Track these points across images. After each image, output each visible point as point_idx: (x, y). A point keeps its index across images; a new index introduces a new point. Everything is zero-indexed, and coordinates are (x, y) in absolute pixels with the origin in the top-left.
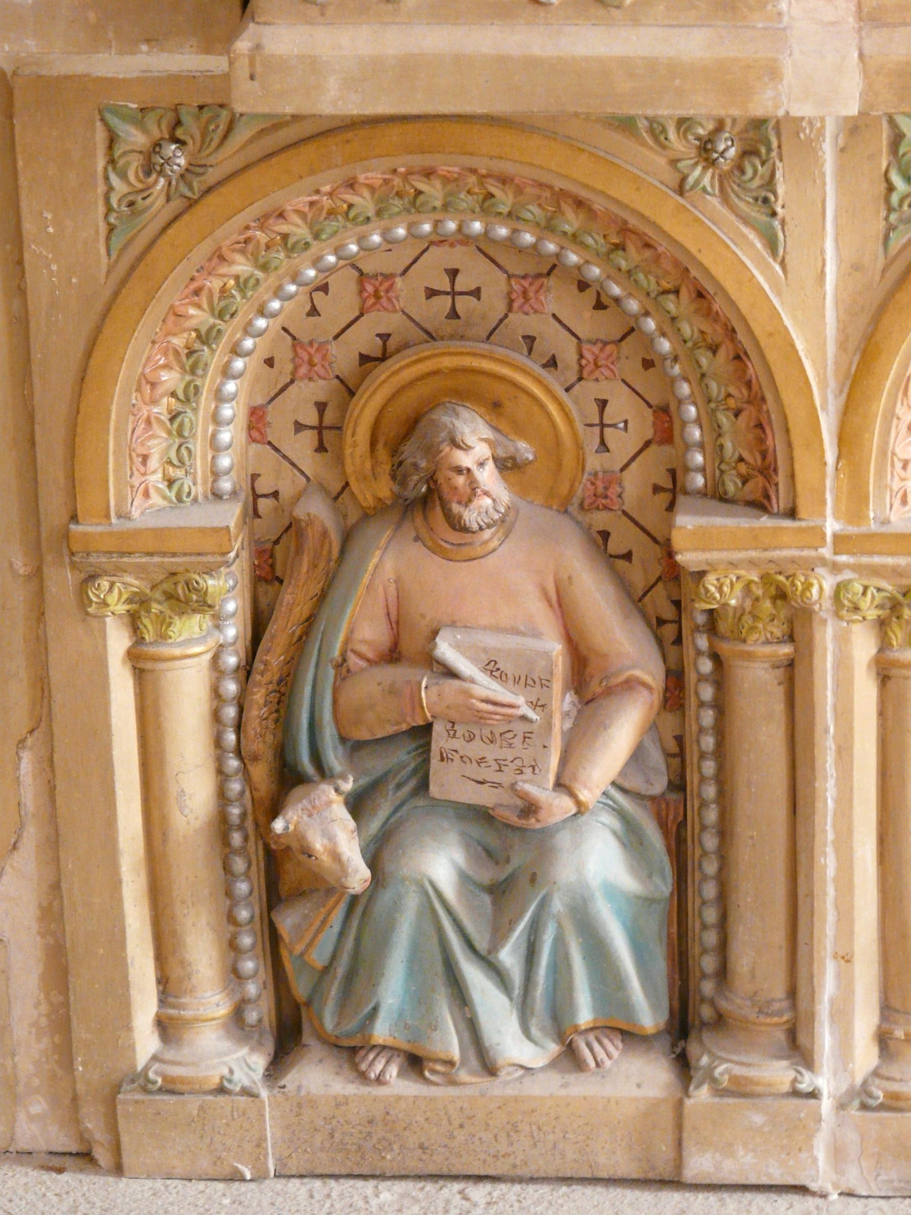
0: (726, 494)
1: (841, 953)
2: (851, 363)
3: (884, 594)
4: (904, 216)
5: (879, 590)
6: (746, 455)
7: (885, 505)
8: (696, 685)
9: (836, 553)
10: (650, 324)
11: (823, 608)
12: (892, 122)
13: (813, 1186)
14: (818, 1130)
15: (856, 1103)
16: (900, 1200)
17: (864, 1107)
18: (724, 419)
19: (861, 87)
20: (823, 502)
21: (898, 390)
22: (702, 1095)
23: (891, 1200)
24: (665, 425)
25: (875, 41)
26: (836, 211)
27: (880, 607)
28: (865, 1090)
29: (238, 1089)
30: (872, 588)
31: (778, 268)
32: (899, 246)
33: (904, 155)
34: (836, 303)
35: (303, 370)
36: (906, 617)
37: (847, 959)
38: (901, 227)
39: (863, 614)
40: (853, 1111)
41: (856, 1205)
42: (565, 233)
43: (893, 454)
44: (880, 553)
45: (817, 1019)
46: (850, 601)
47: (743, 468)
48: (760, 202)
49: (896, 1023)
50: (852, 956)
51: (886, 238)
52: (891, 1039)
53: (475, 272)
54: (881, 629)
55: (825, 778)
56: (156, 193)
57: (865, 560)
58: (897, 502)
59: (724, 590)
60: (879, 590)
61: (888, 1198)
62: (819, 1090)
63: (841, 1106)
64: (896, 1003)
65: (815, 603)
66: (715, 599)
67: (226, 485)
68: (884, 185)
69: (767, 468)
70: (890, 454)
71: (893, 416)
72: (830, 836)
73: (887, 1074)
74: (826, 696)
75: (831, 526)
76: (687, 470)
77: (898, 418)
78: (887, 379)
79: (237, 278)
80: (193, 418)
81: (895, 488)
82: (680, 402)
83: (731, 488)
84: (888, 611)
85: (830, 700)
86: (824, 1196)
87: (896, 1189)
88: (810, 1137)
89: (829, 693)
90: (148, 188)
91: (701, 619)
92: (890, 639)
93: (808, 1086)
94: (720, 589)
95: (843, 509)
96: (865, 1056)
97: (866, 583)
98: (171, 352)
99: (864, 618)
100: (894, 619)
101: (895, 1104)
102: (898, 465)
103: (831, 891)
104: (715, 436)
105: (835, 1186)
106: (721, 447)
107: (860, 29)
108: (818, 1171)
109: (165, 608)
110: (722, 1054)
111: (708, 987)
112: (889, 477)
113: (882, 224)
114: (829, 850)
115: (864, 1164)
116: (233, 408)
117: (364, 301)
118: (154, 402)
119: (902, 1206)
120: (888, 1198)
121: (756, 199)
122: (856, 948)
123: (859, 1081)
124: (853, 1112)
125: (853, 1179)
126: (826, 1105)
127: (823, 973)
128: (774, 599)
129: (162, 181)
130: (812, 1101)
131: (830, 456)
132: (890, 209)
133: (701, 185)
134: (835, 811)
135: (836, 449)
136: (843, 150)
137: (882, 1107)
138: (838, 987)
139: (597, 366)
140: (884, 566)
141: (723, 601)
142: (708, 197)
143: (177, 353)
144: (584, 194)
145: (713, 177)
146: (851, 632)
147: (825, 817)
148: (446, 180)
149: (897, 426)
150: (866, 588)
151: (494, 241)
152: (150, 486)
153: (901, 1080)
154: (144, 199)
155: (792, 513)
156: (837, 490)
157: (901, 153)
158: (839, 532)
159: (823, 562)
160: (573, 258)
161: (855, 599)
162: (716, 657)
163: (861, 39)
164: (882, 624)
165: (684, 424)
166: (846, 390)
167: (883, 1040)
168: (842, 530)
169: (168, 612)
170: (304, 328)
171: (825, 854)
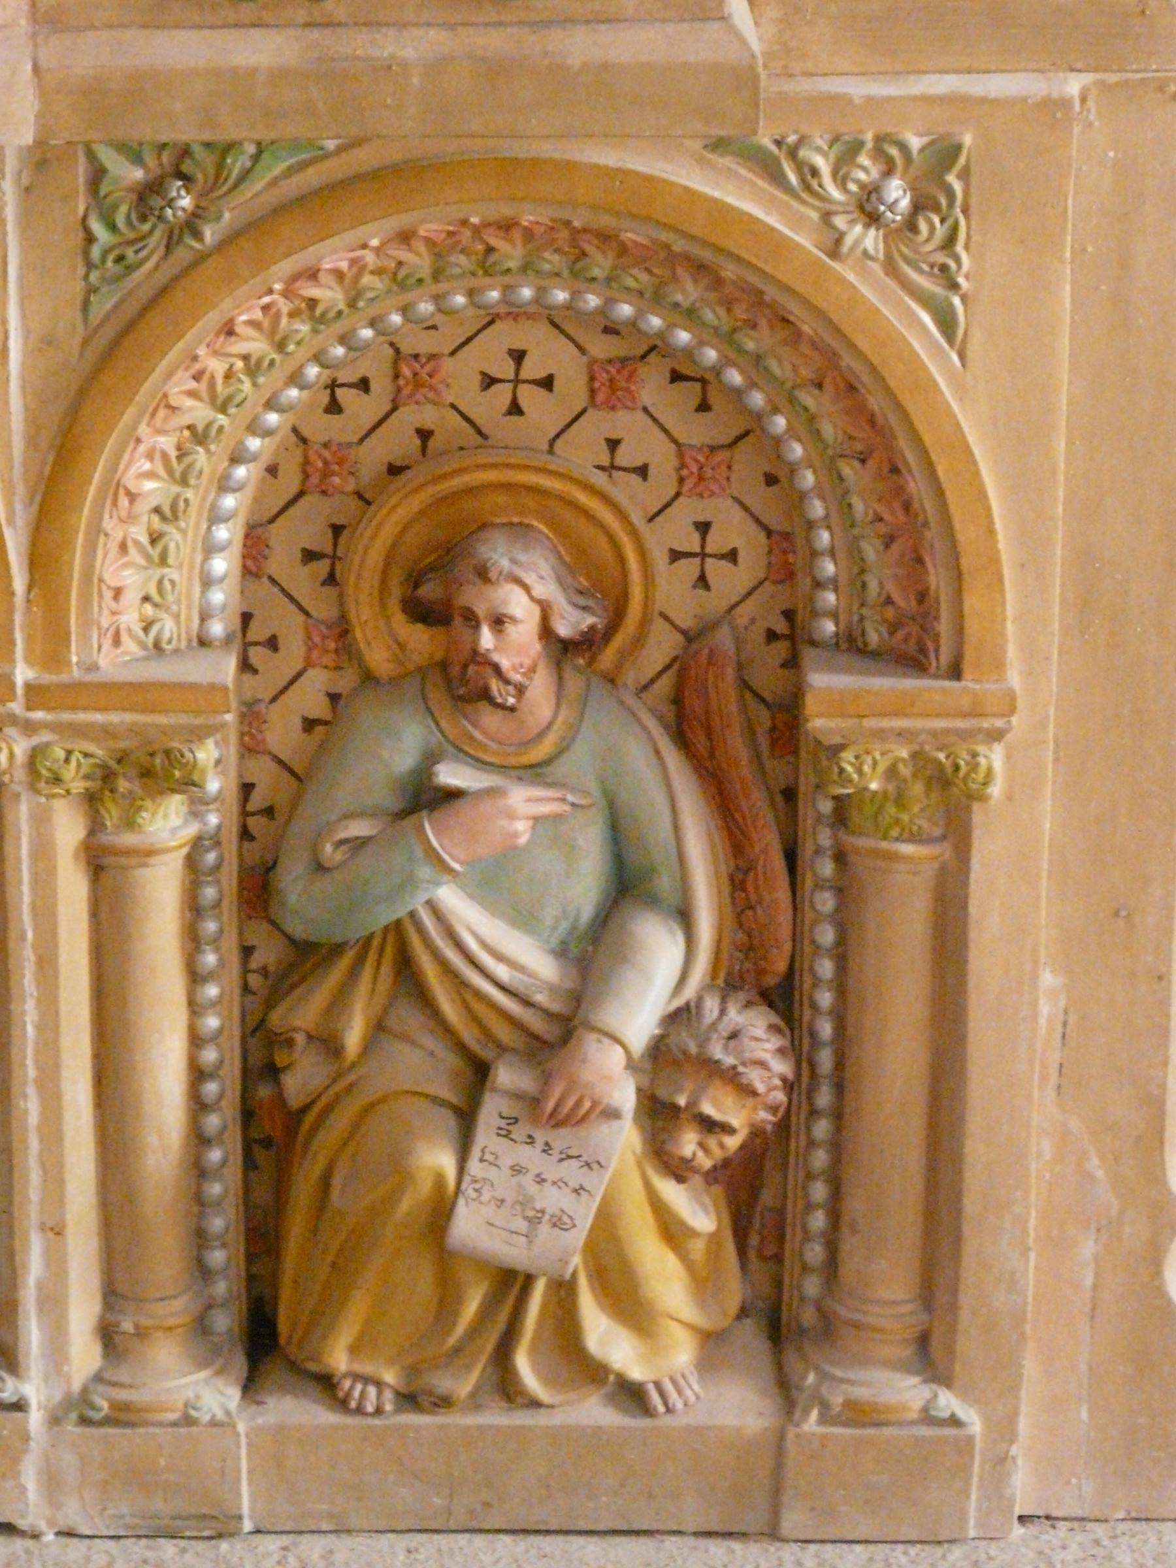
0: (866, 644)
1: (49, 1224)
2: (44, 463)
3: (92, 761)
4: (108, 274)
5: (86, 755)
6: (897, 597)
7: (91, 647)
8: (813, 891)
9: (29, 709)
10: (780, 423)
11: (16, 779)
12: (91, 155)
13: (22, 1524)
14: (26, 1452)
15: (74, 1416)
16: (133, 1540)
17: (84, 1421)
18: (870, 550)
19: (36, 108)
20: (12, 642)
21: (105, 498)
22: (811, 1423)
23: (123, 1541)
24: (786, 552)
25: (53, 51)
26: (21, 268)
27: (87, 777)
28: (85, 1398)
29: (207, 1418)
30: (77, 753)
31: (955, 357)
32: (102, 314)
33: (105, 197)
34: (23, 388)
35: (689, 484)
36: (121, 790)
37: (58, 1231)
38: (105, 289)
39: (66, 786)
40: (71, 1428)
41: (76, 1549)
42: (677, 305)
43: (101, 580)
44: (85, 709)
45: (20, 1309)
46: (50, 770)
47: (890, 613)
48: (936, 270)
49: (121, 1312)
50: (64, 1226)
51: (86, 305)
52: (117, 1333)
53: (548, 353)
54: (91, 807)
55: (23, 998)
56: (151, 246)
57: (66, 716)
58: (107, 643)
59: (867, 773)
60: (86, 755)
61: (120, 1537)
62: (26, 1400)
63: (55, 1420)
64: (122, 1288)
65: (4, 773)
66: (851, 781)
67: (217, 629)
68: (81, 235)
69: (925, 615)
70: (96, 581)
71: (99, 532)
72: (32, 1073)
73: (114, 1379)
74: (21, 893)
75: (22, 674)
76: (815, 614)
77: (106, 535)
78: (90, 483)
79: (246, 358)
80: (181, 542)
81: (105, 623)
82: (810, 525)
83: (873, 638)
84: (99, 782)
85: (26, 899)
86: (36, 1536)
87: (127, 1527)
88: (16, 1461)
89: (26, 889)
90: (143, 238)
91: (826, 807)
92: (103, 817)
93: (12, 1394)
94: (860, 771)
95: (38, 651)
96: (84, 1356)
97: (69, 746)
98: (158, 456)
99: (68, 792)
100: (107, 793)
101: (123, 1417)
102: (108, 595)
103: (34, 1143)
104: (856, 570)
105: (51, 1522)
106: (864, 586)
107: (34, 36)
108: (27, 1505)
109: (136, 787)
110: (839, 1373)
111: (812, 1286)
112: (96, 609)
113: (79, 287)
114: (31, 1091)
115: (86, 1496)
116: (228, 530)
117: (399, 390)
118: (131, 518)
119: (136, 1549)
120: (120, 1537)
121: (932, 266)
122: (68, 1217)
123: (76, 1386)
124: (69, 1428)
125: (73, 1514)
126: (35, 1419)
127: (26, 1250)
128: (929, 781)
129: (161, 228)
130: (18, 1415)
131: (19, 584)
132: (90, 265)
133: (862, 247)
134: (37, 1043)
135: (26, 575)
136: (27, 190)
137: (107, 1421)
138: (48, 1266)
139: (701, 478)
140: (93, 725)
141: (863, 784)
142: (870, 263)
143: (165, 456)
144: (706, 255)
145: (876, 238)
146: (50, 809)
147: (24, 1051)
148: (528, 234)
149: (105, 545)
150: (69, 753)
151: (580, 313)
152: (122, 627)
153: (131, 1387)
154: (136, 252)
155: (956, 672)
156: (29, 626)
157: (102, 193)
158: (32, 682)
159: (13, 720)
160: (683, 337)
161: (55, 767)
162: (840, 857)
163: (36, 46)
164: (92, 800)
165: (814, 554)
166: (38, 499)
167: (108, 1335)
168: (36, 678)
169: (140, 792)
170: (322, 428)
171: (25, 1097)
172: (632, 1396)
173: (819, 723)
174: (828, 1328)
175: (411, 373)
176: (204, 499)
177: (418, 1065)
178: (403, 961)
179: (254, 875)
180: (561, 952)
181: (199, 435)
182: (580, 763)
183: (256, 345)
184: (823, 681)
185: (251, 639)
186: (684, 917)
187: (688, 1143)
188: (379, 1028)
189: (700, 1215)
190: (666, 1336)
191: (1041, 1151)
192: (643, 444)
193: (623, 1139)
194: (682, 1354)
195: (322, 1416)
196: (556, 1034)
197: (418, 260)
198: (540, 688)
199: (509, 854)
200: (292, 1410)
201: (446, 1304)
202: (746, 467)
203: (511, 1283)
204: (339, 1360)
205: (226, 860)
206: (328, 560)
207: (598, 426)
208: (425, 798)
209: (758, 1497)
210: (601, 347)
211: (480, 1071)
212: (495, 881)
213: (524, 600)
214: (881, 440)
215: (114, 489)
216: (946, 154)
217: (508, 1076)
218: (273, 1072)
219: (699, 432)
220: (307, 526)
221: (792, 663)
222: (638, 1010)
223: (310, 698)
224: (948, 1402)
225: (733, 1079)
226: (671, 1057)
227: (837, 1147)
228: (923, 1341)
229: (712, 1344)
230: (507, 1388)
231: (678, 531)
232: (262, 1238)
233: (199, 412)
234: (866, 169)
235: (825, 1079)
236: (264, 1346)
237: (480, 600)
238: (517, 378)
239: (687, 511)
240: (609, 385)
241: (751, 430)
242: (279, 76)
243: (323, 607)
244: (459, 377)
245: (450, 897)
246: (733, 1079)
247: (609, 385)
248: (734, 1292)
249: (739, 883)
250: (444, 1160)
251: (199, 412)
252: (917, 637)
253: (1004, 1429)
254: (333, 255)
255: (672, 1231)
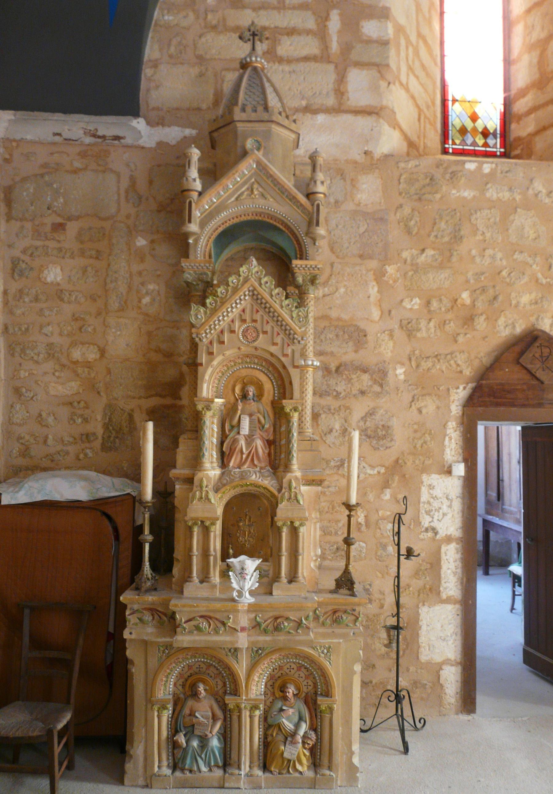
24: (315, 684)
53: (293, 666)
59: (323, 707)
75: (244, 698)
96: (248, 769)
164: (250, 711)
170: (272, 673)
172: (301, 773)
173: (319, 702)
174: (320, 765)
175: (281, 668)
176: (237, 190)
177: (281, 738)
178: (279, 727)
179: (265, 718)
180: (294, 726)
181: (261, 674)
182: (296, 707)
183: (266, 665)
184: (319, 698)
185: (265, 694)
186: (306, 722)
187: (306, 746)
188: (277, 734)
189: (308, 754)
190: (304, 767)
191: (340, 746)
192: (302, 675)
193: (300, 745)
194: (306, 769)
195: (271, 775)
196: (294, 734)
197: (281, 657)
198: (292, 699)
199: (289, 716)
200: (268, 775)
201: (283, 762)
202: (312, 676)
203: (289, 761)
204: (272, 769)
205: (262, 716)
206: (272, 686)
207: (298, 673)
208: (281, 710)
209: (313, 785)
210: (298, 665)
211: (286, 738)
212: (288, 719)
213: (291, 690)
214: (324, 675)
215: (253, 679)
216: (330, 647)
217: (289, 739)
218: (266, 738)
219: (307, 673)
220: (270, 683)
221: (316, 696)
222: (301, 732)
223: (271, 700)
224: (332, 773)
225: (310, 739)
226: (305, 737)
227: (320, 745)
228: (329, 767)
229: (309, 767)
230: (288, 772)
231: (305, 683)
232: (265, 756)
233: (261, 672)
234: (323, 649)
235: (319, 739)
236: (265, 768)
237: (287, 690)
238: (290, 668)
239: (306, 681)
240: (299, 669)
241: (312, 673)
242: (270, 641)
243: (272, 690)
244: (285, 668)
245: (284, 720)
246: (310, 739)
247: (299, 669)
248: (311, 761)
249: (311, 718)
250: (283, 748)
251: (261, 672)
252: (328, 694)
253: (337, 777)
254: (274, 657)
255: (305, 755)
